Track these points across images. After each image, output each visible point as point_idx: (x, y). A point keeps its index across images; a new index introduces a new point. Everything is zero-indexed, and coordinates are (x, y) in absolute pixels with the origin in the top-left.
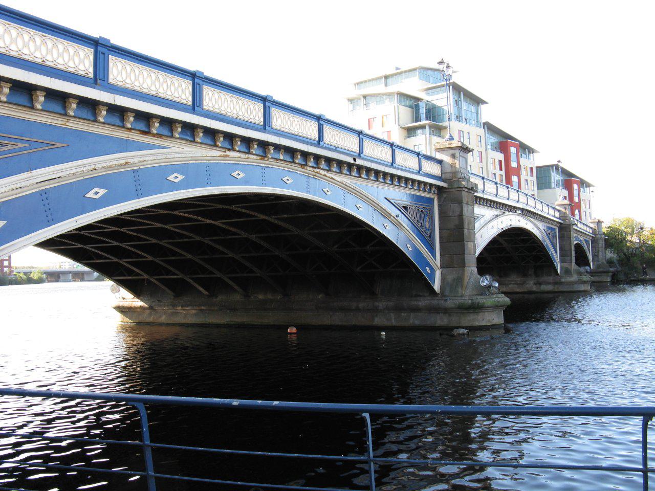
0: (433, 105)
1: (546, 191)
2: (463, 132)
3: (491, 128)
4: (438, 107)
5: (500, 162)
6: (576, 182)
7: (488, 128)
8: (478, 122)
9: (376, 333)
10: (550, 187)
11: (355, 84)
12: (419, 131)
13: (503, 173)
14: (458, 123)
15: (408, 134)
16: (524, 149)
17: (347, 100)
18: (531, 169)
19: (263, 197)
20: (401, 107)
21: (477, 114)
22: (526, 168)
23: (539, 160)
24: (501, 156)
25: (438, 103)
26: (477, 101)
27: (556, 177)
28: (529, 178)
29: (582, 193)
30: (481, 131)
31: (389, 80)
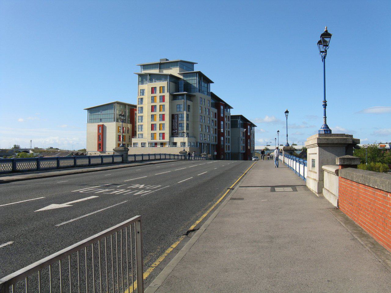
0: (187, 82)
1: (236, 129)
2: (202, 98)
3: (213, 96)
4: (191, 84)
5: (215, 113)
6: (222, 105)
7: (211, 96)
8: (207, 92)
9: (346, 208)
10: (237, 127)
11: (141, 66)
12: (180, 97)
13: (216, 120)
14: (199, 93)
15: (174, 98)
16: (227, 107)
17: (137, 76)
18: (229, 117)
19: (235, 180)
20: (171, 83)
21: (208, 88)
22: (226, 116)
23: (233, 112)
24: (215, 111)
25: (190, 82)
26: (208, 81)
27: (240, 121)
28: (228, 122)
29: (225, 112)
30: (209, 98)
31: (162, 66)
